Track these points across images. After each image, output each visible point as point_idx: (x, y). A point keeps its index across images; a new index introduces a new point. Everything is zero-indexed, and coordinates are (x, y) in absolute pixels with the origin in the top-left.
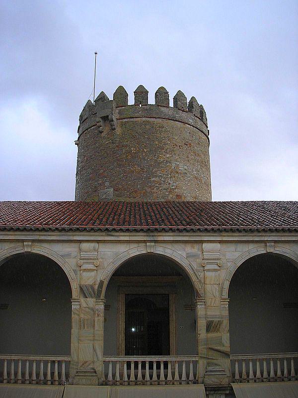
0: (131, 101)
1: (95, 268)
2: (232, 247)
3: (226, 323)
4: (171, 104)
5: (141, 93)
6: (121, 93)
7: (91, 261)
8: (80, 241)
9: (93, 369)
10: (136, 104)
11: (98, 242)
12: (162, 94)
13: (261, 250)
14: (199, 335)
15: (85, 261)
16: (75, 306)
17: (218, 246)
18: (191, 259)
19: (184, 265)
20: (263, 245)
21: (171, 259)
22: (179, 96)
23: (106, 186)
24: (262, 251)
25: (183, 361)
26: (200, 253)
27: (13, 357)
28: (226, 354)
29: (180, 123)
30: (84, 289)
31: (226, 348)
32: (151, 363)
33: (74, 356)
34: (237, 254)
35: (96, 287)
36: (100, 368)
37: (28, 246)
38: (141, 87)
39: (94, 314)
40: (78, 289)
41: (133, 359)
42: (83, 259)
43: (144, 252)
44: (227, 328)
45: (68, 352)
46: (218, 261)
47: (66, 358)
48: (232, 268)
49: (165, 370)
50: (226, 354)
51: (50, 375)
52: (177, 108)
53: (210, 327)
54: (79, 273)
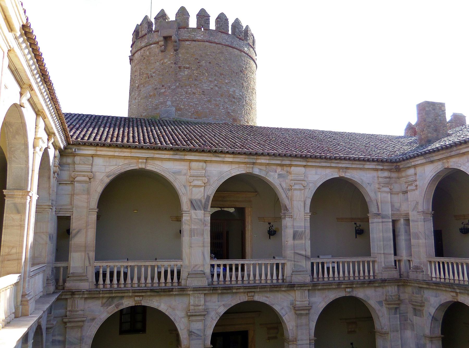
0: (193, 23)
3: (308, 231)
4: (230, 32)
5: (203, 16)
6: (183, 13)
7: (201, 178)
8: (191, 161)
10: (199, 28)
11: (205, 162)
12: (222, 19)
13: (336, 175)
14: (286, 242)
15: (296, 182)
16: (185, 218)
17: (303, 169)
18: (281, 179)
19: (276, 184)
20: (337, 170)
22: (237, 23)
23: (167, 105)
24: (336, 175)
25: (251, 264)
28: (306, 257)
29: (237, 51)
30: (194, 202)
31: (309, 253)
32: (231, 266)
33: (186, 262)
34: (317, 177)
35: (203, 201)
36: (208, 270)
37: (142, 163)
38: (222, 14)
40: (189, 203)
42: (193, 176)
43: (244, 172)
44: (309, 237)
45: (179, 257)
46: (303, 182)
48: (312, 189)
49: (243, 273)
52: (235, 35)
53: (295, 236)
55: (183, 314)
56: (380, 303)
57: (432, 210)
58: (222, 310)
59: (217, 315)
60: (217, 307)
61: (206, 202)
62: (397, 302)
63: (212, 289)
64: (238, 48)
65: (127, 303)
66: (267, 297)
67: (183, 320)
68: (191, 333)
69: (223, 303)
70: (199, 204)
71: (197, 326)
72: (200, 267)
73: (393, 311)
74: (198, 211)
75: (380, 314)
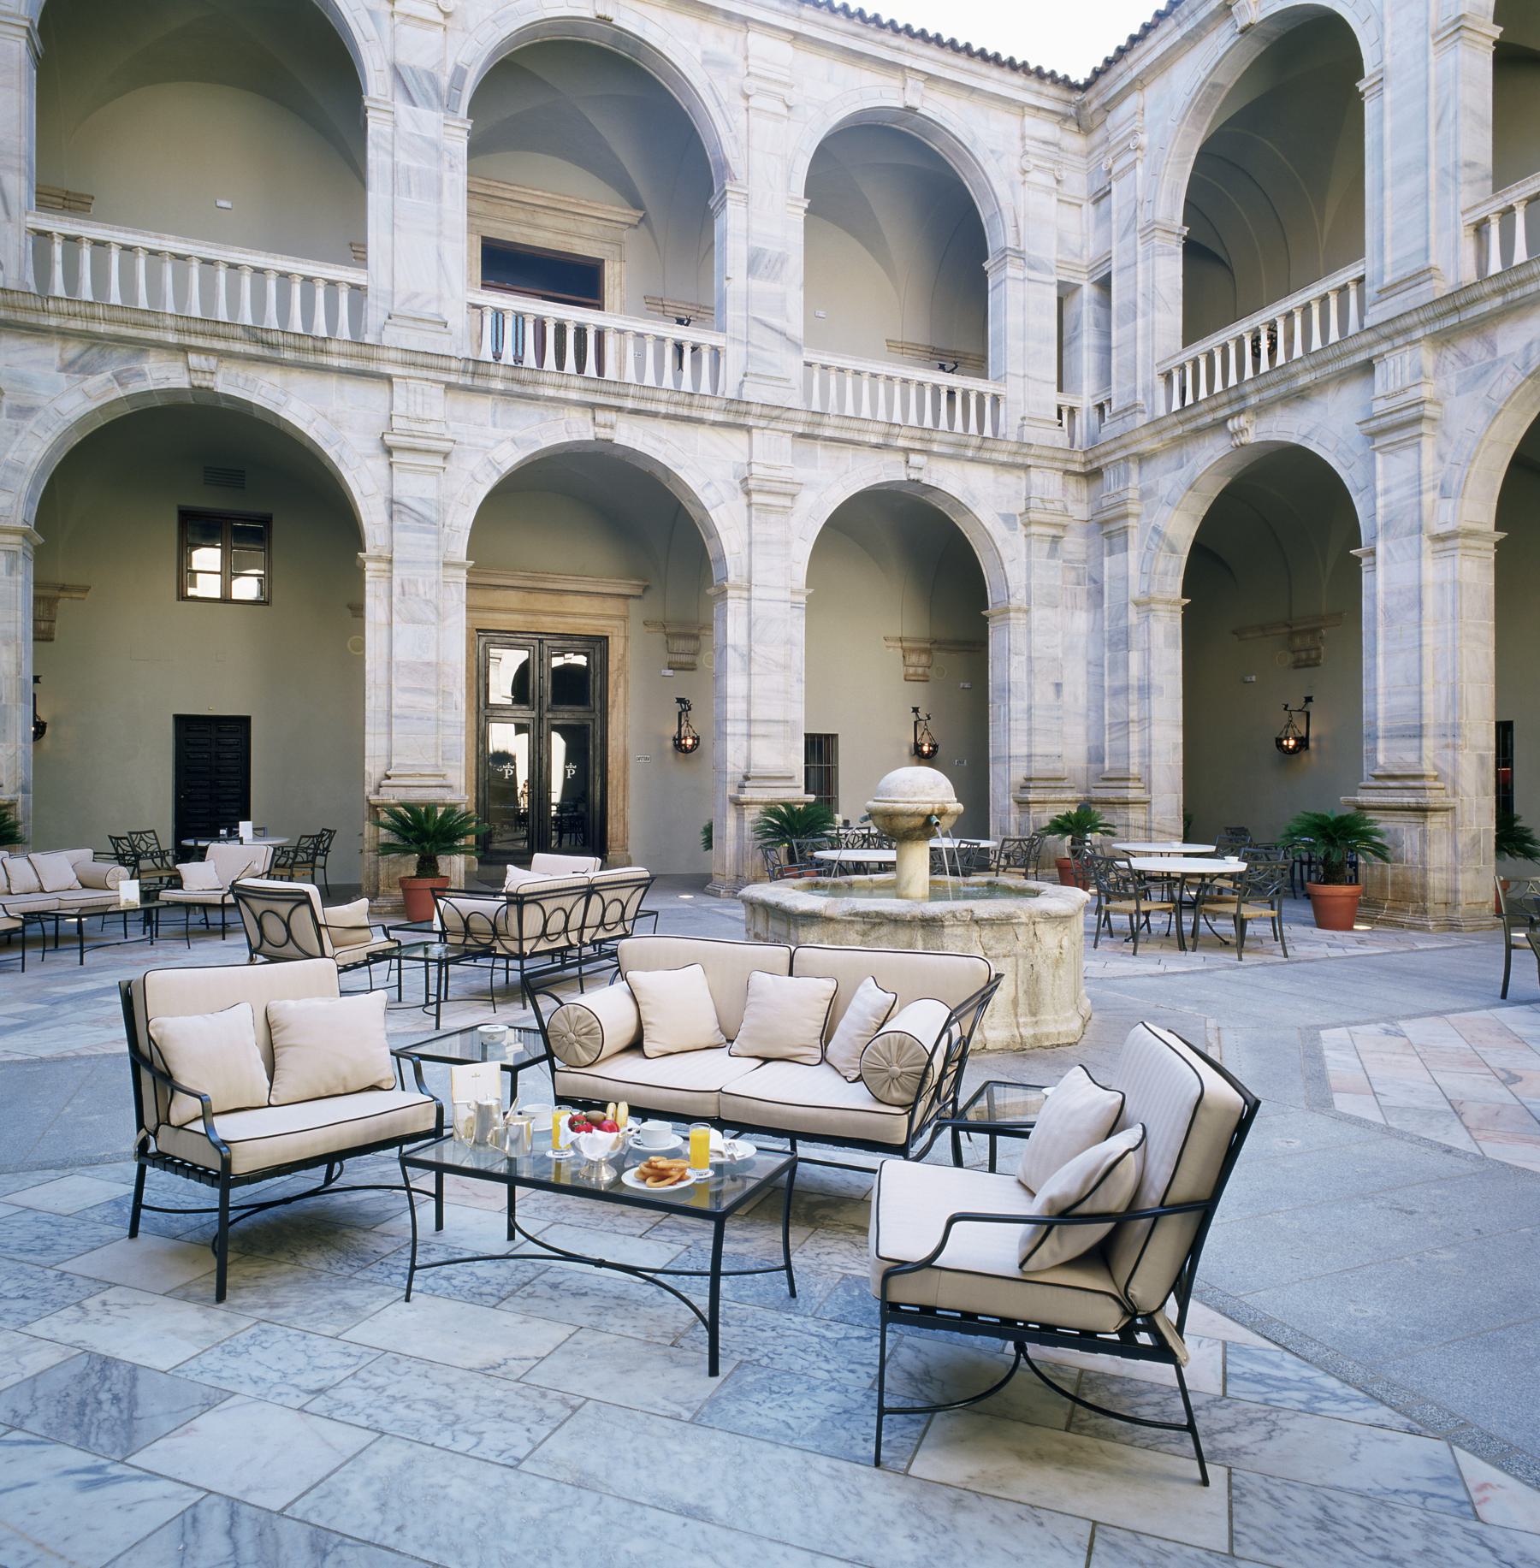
1: (440, 18)
2: (818, 65)
9: (439, 315)
21: (127, 410)
26: (738, 59)
27: (171, 244)
30: (408, 77)
31: (796, 329)
35: (445, 81)
39: (440, 157)
40: (388, 75)
41: (48, 223)
45: (357, 253)
47: (347, 275)
50: (797, 346)
51: (631, 173)
53: (754, 264)
54: (386, 23)
55: (371, 446)
56: (1008, 519)
57: (1185, 224)
58: (510, 458)
59: (490, 468)
60: (491, 443)
61: (451, 86)
62: (1058, 519)
63: (470, 380)
64: (458, 1257)
65: (162, 375)
66: (660, 440)
67: (369, 463)
68: (394, 506)
69: (511, 433)
70: (427, 85)
71: (414, 486)
72: (429, 302)
73: (1046, 546)
74: (422, 112)
75: (1006, 553)
